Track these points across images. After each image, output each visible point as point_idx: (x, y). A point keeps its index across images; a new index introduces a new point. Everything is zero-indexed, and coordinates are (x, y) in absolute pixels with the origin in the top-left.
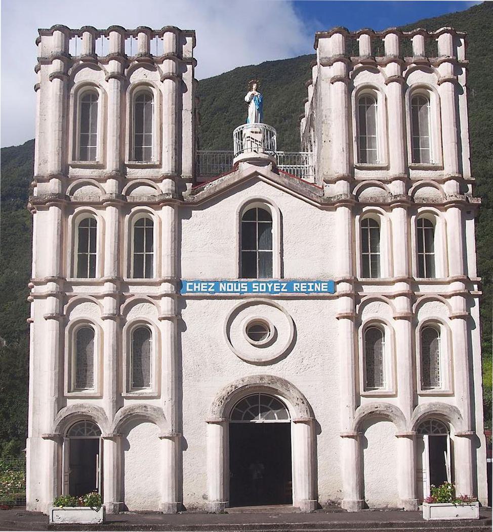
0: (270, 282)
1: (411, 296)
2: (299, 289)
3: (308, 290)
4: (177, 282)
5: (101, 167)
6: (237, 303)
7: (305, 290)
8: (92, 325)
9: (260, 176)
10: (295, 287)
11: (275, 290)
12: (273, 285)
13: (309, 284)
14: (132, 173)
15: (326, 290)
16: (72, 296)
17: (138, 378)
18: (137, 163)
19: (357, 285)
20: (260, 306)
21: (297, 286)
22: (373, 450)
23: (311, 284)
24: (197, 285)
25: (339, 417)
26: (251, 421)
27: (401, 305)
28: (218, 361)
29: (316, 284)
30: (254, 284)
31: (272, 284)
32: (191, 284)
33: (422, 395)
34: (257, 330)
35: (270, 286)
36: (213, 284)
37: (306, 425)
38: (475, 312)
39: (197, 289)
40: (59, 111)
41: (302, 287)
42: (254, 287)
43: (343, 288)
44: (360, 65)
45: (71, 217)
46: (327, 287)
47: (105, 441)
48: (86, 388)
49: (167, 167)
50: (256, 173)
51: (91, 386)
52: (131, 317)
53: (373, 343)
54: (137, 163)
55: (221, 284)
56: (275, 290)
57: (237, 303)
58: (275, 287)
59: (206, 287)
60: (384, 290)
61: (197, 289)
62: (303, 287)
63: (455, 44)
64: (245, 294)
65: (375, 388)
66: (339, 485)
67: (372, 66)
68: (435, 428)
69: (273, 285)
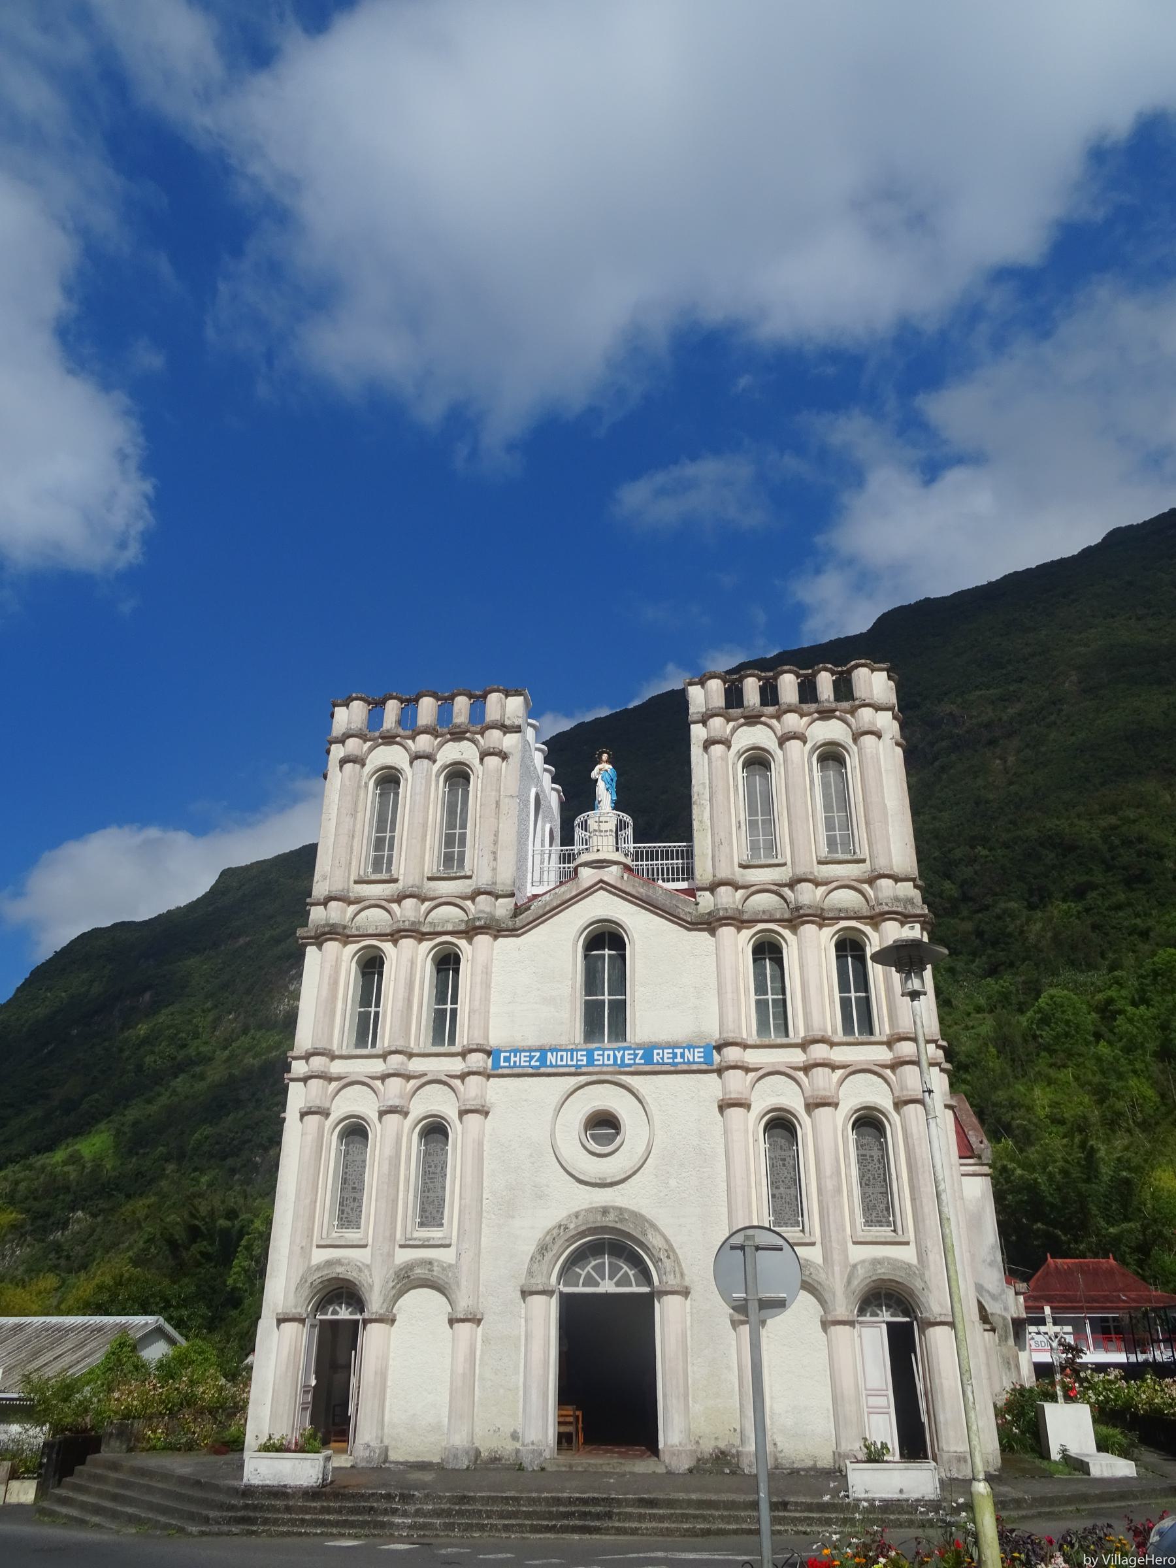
0: (619, 1049)
2: (662, 1059)
11: (627, 1061)
23: (679, 1051)
35: (619, 1055)
41: (666, 1056)
55: (549, 1054)
56: (627, 1061)
58: (627, 1057)
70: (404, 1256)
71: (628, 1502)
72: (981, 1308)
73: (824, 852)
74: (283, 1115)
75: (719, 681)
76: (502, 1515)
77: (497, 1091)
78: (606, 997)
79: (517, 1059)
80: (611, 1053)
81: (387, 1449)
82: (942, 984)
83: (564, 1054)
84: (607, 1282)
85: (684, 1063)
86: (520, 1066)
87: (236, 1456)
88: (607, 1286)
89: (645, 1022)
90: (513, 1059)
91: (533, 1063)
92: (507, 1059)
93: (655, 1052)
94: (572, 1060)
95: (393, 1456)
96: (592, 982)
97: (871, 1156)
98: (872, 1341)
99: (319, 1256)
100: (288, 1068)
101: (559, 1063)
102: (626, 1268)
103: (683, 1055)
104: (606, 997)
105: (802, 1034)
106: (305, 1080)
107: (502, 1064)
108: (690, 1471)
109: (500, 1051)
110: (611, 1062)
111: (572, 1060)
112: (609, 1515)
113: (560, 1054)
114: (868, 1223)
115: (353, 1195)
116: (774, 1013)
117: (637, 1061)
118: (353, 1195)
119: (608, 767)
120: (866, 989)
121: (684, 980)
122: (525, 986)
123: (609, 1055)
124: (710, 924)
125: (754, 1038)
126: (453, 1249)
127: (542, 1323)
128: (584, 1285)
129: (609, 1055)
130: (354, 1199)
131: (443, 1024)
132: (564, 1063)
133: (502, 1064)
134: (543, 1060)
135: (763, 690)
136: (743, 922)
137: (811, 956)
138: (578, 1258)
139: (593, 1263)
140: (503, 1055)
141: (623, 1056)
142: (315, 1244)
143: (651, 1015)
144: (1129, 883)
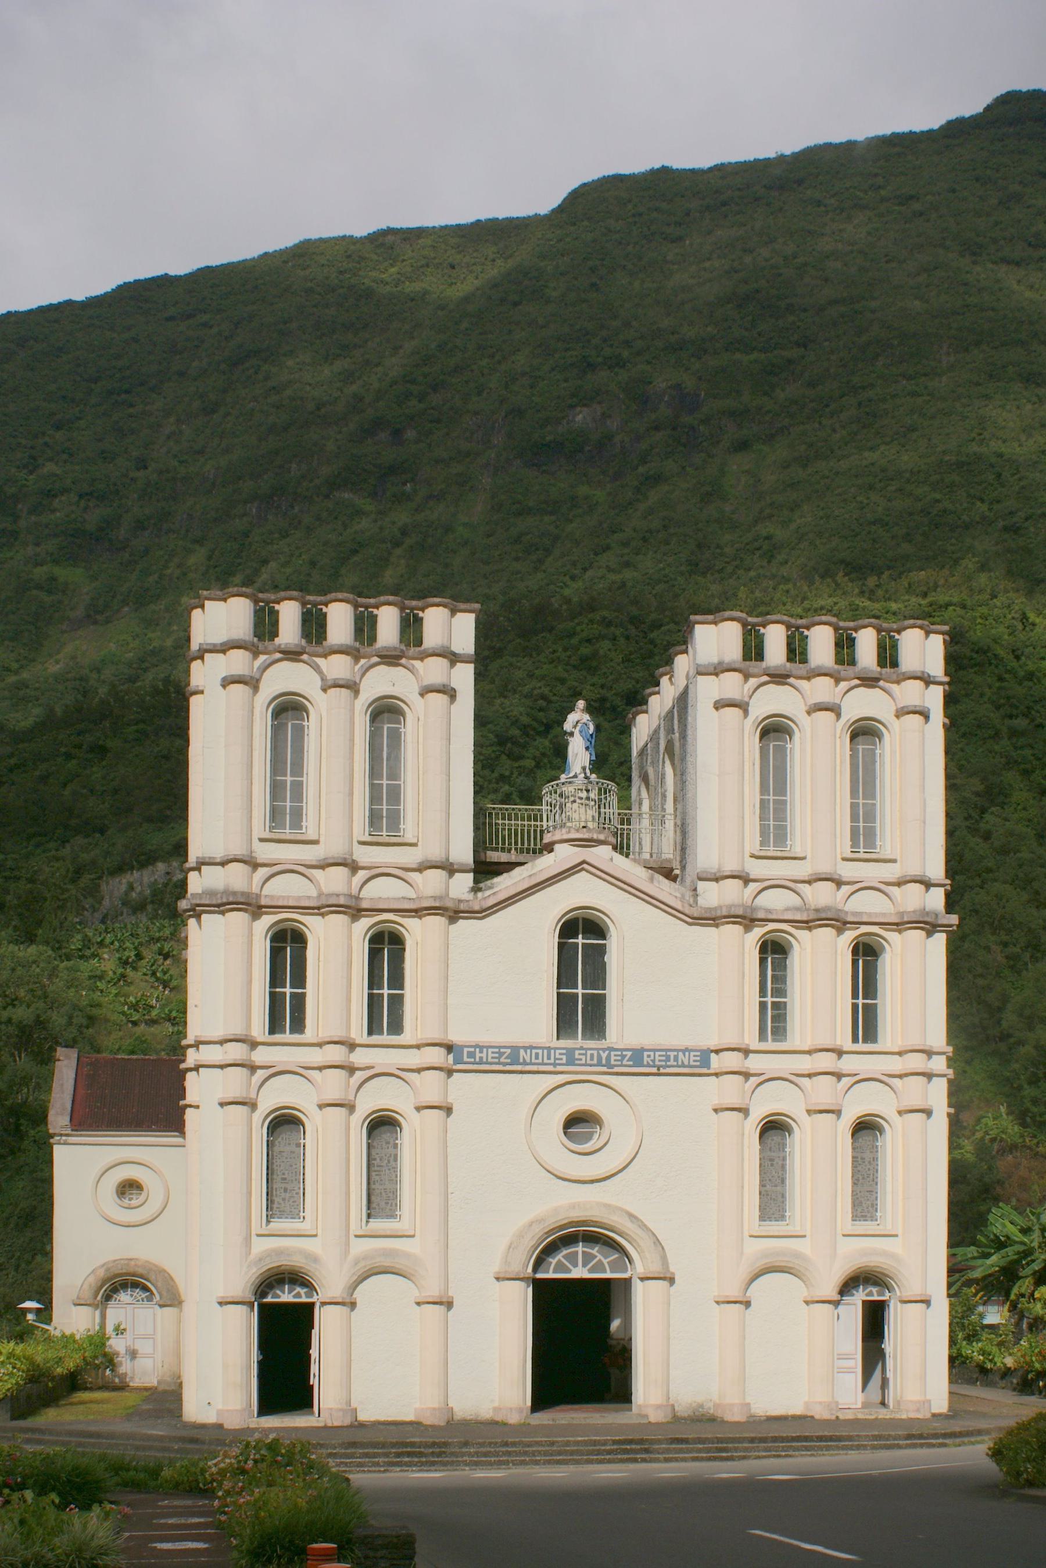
11: (613, 1062)
23: (672, 1054)
35: (604, 1055)
39: (481, 1058)
42: (577, 1056)
55: (522, 1052)
56: (613, 1062)
58: (613, 1058)
64: (559, 1068)
70: (361, 1247)
71: (659, 1442)
73: (756, 848)
74: (952, 1110)
76: (546, 1454)
77: (463, 1088)
78: (580, 991)
79: (484, 1055)
80: (595, 1053)
81: (673, 1406)
83: (540, 1051)
84: (578, 1266)
85: (678, 1066)
86: (487, 1063)
87: (627, 1405)
88: (579, 1272)
89: (628, 1021)
90: (478, 1055)
91: (502, 1060)
93: (646, 1054)
94: (549, 1058)
95: (362, 1417)
96: (565, 975)
97: (862, 1158)
98: (852, 1315)
99: (261, 1246)
100: (951, 1062)
101: (533, 1060)
102: (599, 1257)
103: (676, 1058)
104: (580, 991)
105: (809, 1043)
106: (196, 1068)
109: (463, 1047)
110: (595, 1061)
111: (549, 1058)
112: (398, 1455)
114: (855, 1218)
115: (283, 1185)
116: (774, 1019)
117: (625, 1062)
118: (283, 1185)
119: (586, 717)
120: (272, 995)
121: (675, 978)
122: (489, 973)
124: (712, 919)
125: (365, 1039)
126: (807, 1240)
127: (520, 1301)
128: (555, 1272)
129: (592, 1056)
130: (285, 1190)
131: (384, 1013)
132: (540, 1061)
133: (466, 1059)
134: (515, 1060)
135: (881, 648)
136: (753, 920)
137: (820, 966)
138: (550, 1249)
139: (565, 1252)
140: (466, 1050)
141: (608, 1058)
142: (746, 1234)
143: (634, 1012)
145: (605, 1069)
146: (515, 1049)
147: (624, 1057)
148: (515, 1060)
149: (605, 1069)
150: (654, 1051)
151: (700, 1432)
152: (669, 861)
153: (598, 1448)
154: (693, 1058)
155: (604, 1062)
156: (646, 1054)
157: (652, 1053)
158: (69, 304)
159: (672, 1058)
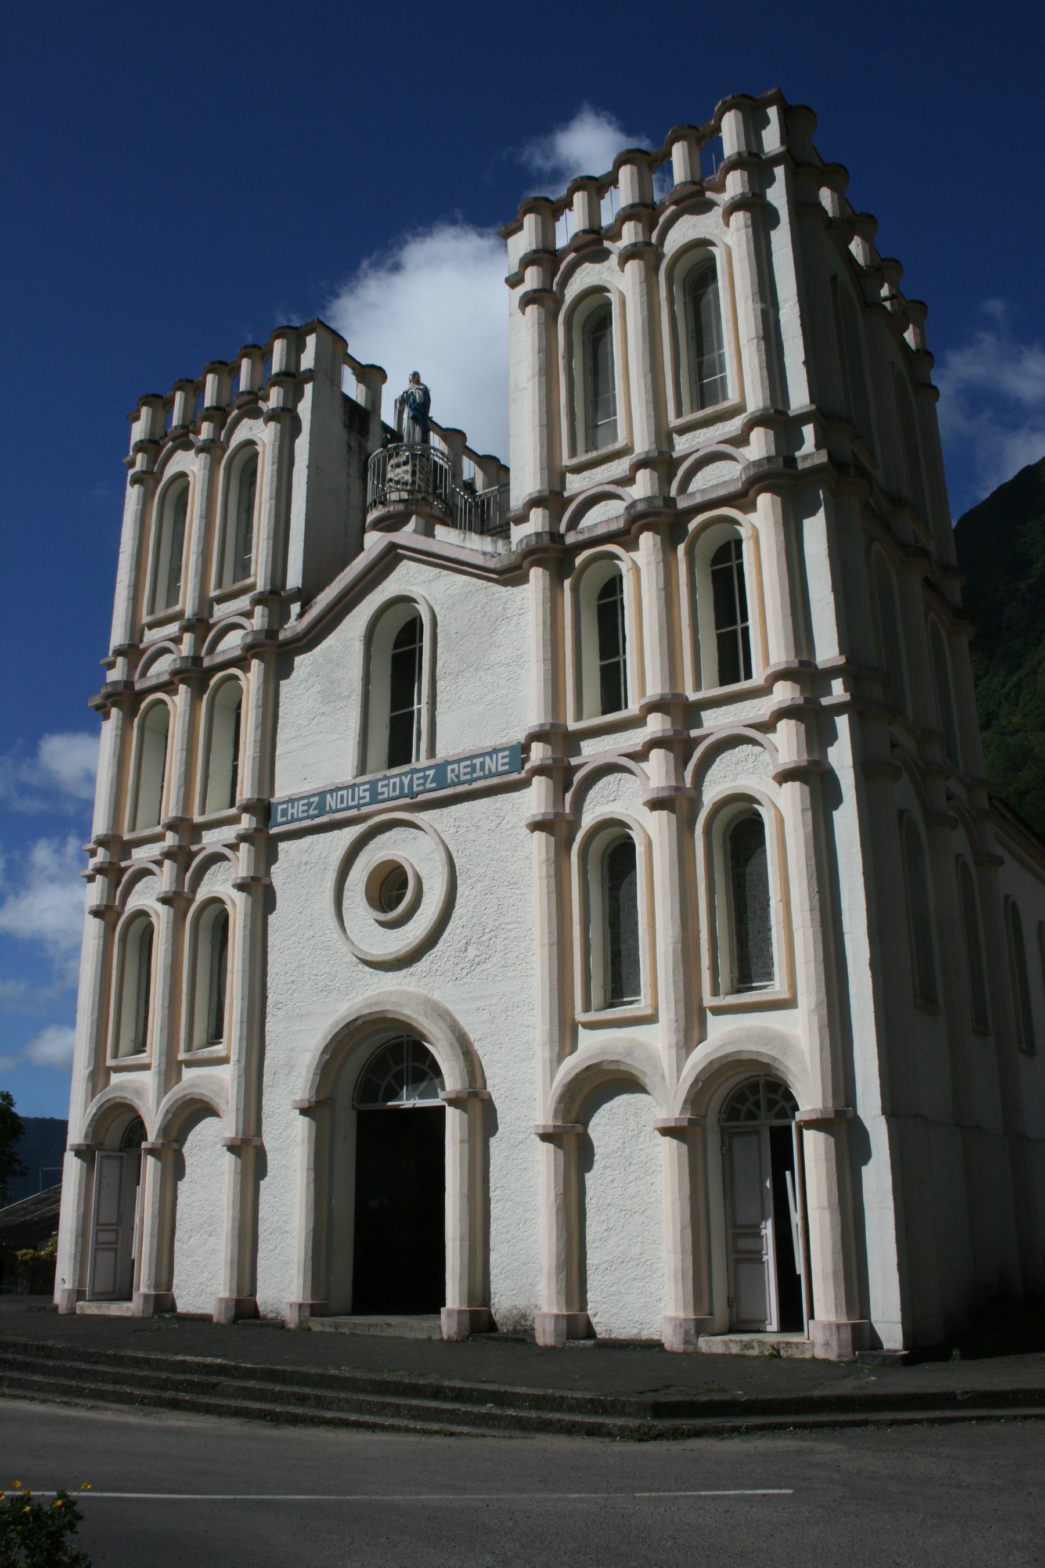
0: (406, 774)
1: (678, 746)
2: (458, 776)
3: (474, 775)
4: (263, 809)
5: (738, 409)
6: (349, 835)
7: (469, 777)
8: (756, 806)
9: (400, 551)
10: (450, 775)
11: (415, 789)
12: (412, 779)
13: (474, 761)
14: (576, 485)
15: (507, 767)
16: (581, 766)
17: (749, 962)
18: (594, 454)
19: (684, 712)
20: (395, 831)
21: (453, 771)
22: (608, 1172)
23: (477, 761)
24: (293, 807)
25: (526, 1089)
26: (389, 1104)
27: (657, 770)
28: (323, 969)
29: (488, 758)
30: (380, 784)
31: (409, 776)
32: (285, 806)
33: (718, 1011)
34: (391, 889)
35: (406, 781)
36: (316, 799)
37: (458, 1111)
38: (841, 756)
39: (292, 814)
40: (134, 538)
41: (463, 770)
42: (380, 790)
43: (538, 753)
44: (573, 255)
45: (681, 548)
46: (507, 760)
47: (809, 1135)
48: (754, 985)
49: (755, 401)
50: (393, 547)
51: (769, 976)
52: (712, 792)
53: (747, 860)
54: (594, 454)
55: (328, 796)
56: (415, 789)
57: (349, 835)
58: (415, 782)
59: (422, 781)
60: (629, 739)
61: (292, 814)
62: (298, 810)
63: (753, 125)
64: (365, 810)
65: (754, 985)
66: (524, 1281)
67: (695, 200)
68: (776, 1102)
69: (412, 779)
72: (761, 745)
75: (645, 534)
79: (295, 811)
82: (695, 1044)
85: (485, 777)
87: (49, 1297)
90: (290, 811)
92: (284, 813)
107: (280, 820)
108: (457, 1341)
110: (397, 793)
111: (353, 799)
113: (340, 793)
123: (394, 784)
132: (344, 805)
133: (280, 820)
134: (322, 809)
144: (492, 1022)
145: (407, 800)
146: (322, 795)
147: (426, 778)
148: (322, 809)
149: (407, 800)
150: (458, 761)
151: (889, 1351)
152: (705, 724)
153: (188, 1377)
154: (498, 764)
155: (406, 791)
156: (449, 768)
157: (456, 766)
158: (871, 959)
159: (478, 766)
